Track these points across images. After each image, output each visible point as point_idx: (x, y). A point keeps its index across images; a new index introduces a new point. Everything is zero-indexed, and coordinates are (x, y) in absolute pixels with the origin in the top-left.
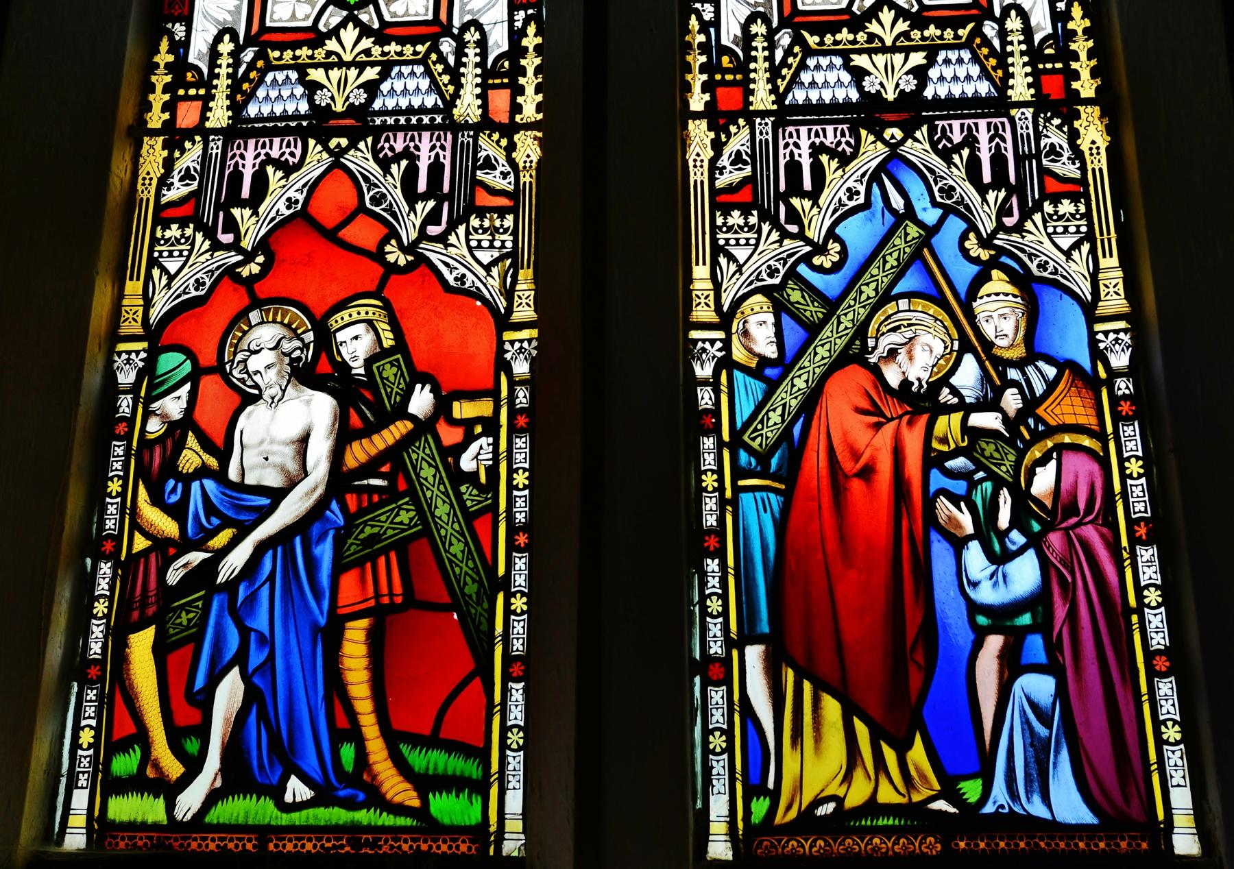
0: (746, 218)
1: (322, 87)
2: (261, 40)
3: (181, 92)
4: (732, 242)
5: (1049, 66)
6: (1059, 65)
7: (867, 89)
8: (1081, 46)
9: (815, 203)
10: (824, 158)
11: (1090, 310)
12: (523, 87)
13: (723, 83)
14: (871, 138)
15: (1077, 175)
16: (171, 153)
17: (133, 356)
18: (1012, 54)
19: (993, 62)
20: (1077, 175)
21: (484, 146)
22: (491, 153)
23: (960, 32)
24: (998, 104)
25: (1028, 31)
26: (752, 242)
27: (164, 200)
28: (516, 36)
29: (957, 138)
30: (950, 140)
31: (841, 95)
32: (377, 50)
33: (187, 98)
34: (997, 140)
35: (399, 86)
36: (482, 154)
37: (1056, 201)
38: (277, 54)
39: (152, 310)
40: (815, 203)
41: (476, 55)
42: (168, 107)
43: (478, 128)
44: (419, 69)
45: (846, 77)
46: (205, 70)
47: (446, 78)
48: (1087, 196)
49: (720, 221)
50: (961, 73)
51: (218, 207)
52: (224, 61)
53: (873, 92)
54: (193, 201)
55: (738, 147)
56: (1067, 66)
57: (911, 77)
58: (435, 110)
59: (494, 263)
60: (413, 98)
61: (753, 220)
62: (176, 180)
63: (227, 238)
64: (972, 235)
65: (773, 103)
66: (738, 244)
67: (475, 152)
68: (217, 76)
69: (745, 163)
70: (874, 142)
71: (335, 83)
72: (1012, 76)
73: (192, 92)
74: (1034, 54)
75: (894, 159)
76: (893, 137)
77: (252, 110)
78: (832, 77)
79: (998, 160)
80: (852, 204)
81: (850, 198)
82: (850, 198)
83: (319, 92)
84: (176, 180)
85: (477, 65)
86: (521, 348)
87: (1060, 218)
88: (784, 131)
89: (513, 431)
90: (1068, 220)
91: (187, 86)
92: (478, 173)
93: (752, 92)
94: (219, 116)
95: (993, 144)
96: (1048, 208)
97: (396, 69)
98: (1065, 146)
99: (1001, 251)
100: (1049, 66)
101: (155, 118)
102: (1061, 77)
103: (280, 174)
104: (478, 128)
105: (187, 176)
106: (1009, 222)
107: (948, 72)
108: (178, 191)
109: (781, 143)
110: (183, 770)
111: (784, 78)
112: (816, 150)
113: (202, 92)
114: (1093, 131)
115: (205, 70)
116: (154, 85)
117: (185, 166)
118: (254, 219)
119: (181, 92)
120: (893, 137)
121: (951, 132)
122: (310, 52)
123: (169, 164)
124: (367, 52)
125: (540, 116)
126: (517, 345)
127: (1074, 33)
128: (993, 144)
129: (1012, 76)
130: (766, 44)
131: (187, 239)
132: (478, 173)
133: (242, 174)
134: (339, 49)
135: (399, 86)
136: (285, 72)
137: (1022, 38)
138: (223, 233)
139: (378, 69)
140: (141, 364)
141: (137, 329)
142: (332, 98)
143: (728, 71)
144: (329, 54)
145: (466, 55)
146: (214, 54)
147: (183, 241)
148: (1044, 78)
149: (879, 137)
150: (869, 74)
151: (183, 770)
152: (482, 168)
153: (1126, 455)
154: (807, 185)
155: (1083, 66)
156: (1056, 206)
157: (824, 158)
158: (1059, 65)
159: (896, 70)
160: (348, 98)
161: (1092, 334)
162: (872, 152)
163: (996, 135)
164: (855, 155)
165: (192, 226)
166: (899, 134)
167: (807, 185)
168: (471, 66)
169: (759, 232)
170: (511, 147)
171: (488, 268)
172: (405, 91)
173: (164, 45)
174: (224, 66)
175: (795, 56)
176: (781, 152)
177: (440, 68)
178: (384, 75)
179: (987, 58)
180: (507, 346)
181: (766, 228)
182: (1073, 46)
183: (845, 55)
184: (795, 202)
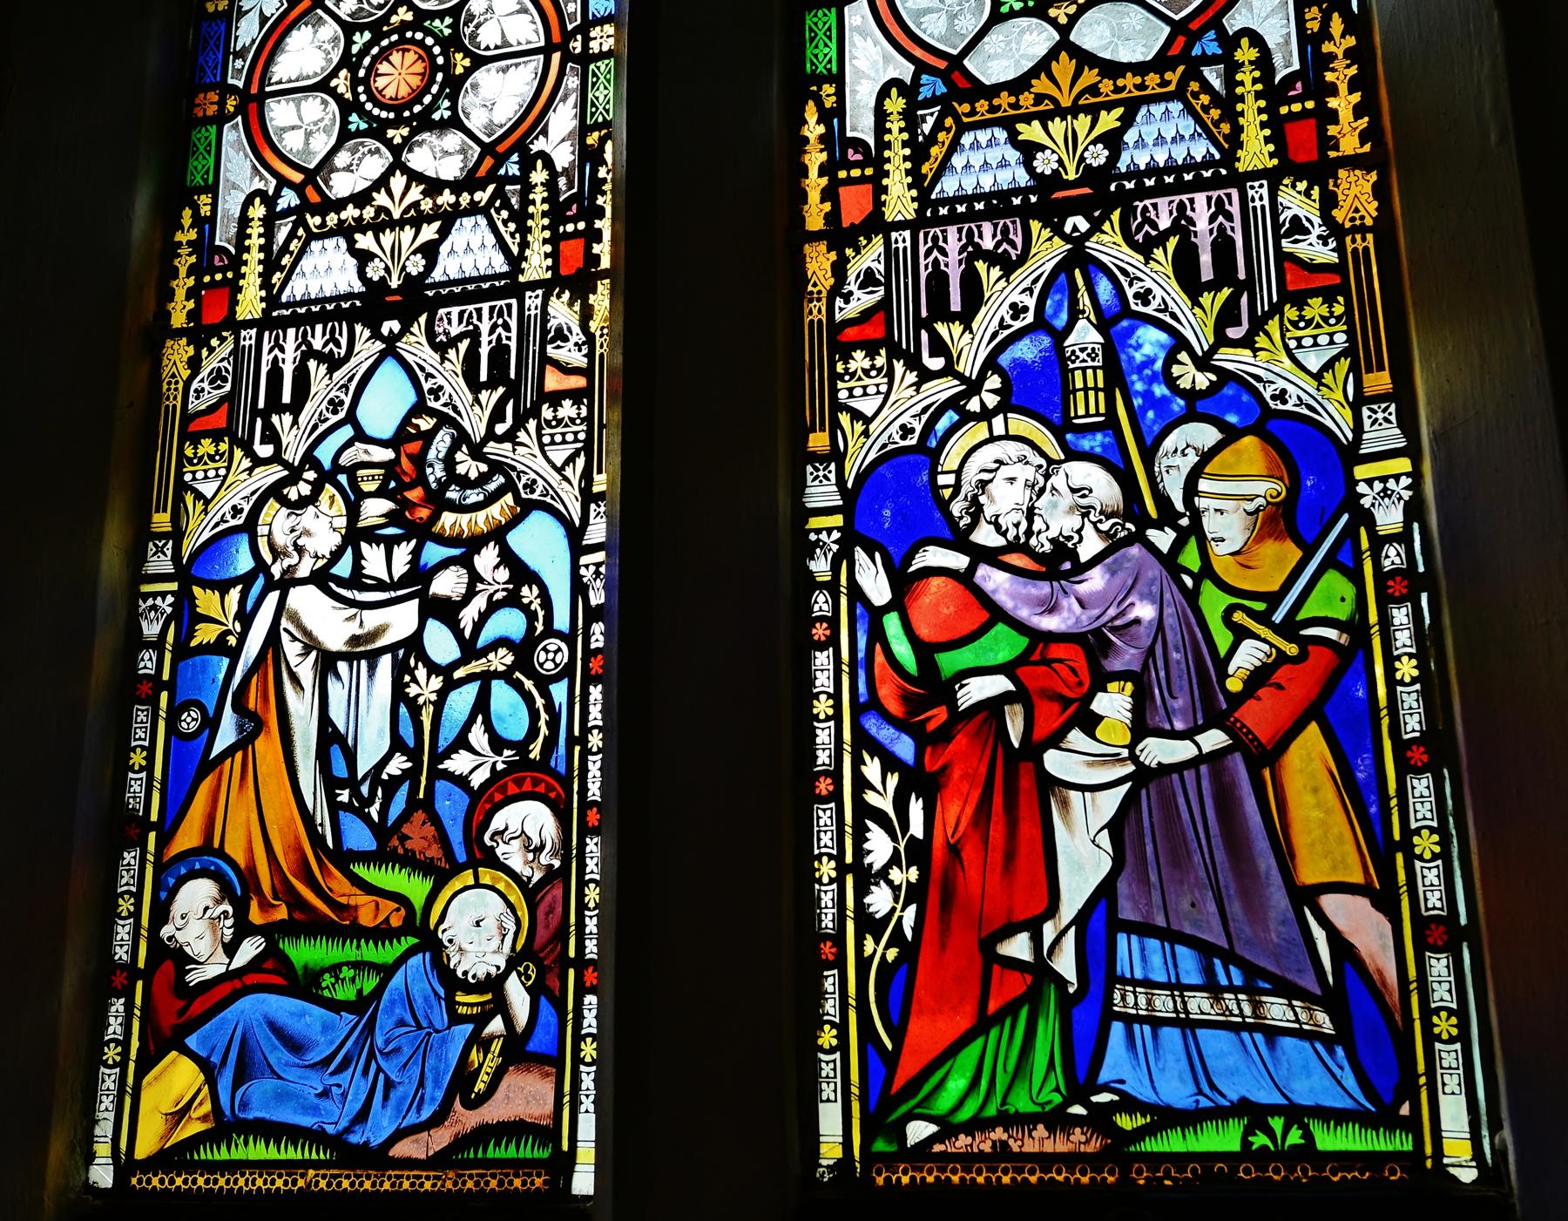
0: (1331, 307)
1: (1043, 148)
2: (946, 91)
3: (842, 174)
4: (1307, 342)
5: (1296, 107)
6: (1310, 105)
7: (1039, 170)
8: (1341, 74)
9: (968, 328)
10: (981, 266)
11: (575, 534)
12: (1335, 112)
13: (850, 181)
14: (1046, 233)
15: (1334, 258)
16: (841, 255)
17: (1391, 484)
18: (1241, 99)
19: (1215, 113)
20: (1334, 258)
21: (1286, 203)
22: (1296, 211)
23: (1168, 76)
24: (1223, 173)
25: (1264, 62)
26: (883, 388)
27: (838, 317)
28: (1309, 42)
29: (1164, 223)
30: (1154, 226)
31: (1004, 179)
32: (1106, 86)
33: (850, 181)
34: (935, 253)
35: (1150, 135)
36: (1286, 215)
37: (1300, 301)
38: (966, 108)
39: (185, 542)
40: (968, 328)
41: (1255, 81)
42: (829, 194)
43: (1273, 178)
44: (1175, 107)
45: (1013, 155)
46: (872, 143)
47: (1215, 113)
48: (1344, 289)
49: (840, 368)
50: (1169, 134)
51: (920, 324)
52: (895, 125)
53: (1048, 172)
54: (880, 316)
55: (868, 264)
56: (1321, 104)
57: (1100, 146)
58: (1208, 163)
59: (1329, 365)
60: (1192, 145)
61: (880, 361)
62: (852, 286)
63: (936, 364)
64: (1183, 356)
65: (1272, 155)
66: (865, 394)
67: (1275, 215)
68: (888, 146)
69: (878, 283)
70: (1050, 239)
71: (1061, 142)
72: (887, 174)
73: (856, 173)
74: (1273, 94)
75: (1078, 258)
76: (1075, 228)
77: (948, 186)
78: (994, 156)
79: (1222, 246)
80: (1018, 325)
81: (1015, 317)
82: (1015, 317)
83: (1039, 155)
84: (853, 287)
85: (905, 144)
86: (1385, 489)
87: (1309, 323)
88: (926, 235)
89: (588, 680)
90: (1318, 326)
91: (850, 165)
92: (1284, 243)
93: (885, 190)
94: (900, 202)
95: (1215, 225)
96: (1291, 313)
97: (1143, 110)
98: (1317, 221)
99: (1225, 376)
100: (1296, 107)
101: (814, 210)
102: (1312, 122)
103: (996, 272)
104: (1273, 178)
105: (868, 280)
106: (1234, 333)
107: (976, 159)
108: (862, 300)
109: (922, 250)
110: (591, 1192)
111: (505, 223)
112: (974, 253)
113: (869, 171)
114: (1357, 193)
115: (872, 143)
116: (806, 167)
117: (865, 267)
118: (967, 336)
119: (842, 174)
120: (1075, 228)
121: (981, 236)
122: (1012, 100)
123: (839, 270)
124: (1093, 90)
125: (1367, 148)
126: (1378, 486)
127: (1332, 57)
128: (1215, 225)
129: (887, 174)
130: (1257, 74)
131: (880, 370)
132: (1284, 241)
133: (946, 276)
134: (1054, 92)
135: (1150, 135)
136: (989, 131)
137: (902, 124)
138: (931, 356)
139: (1119, 111)
140: (835, 547)
141: (169, 568)
142: (1060, 161)
143: (856, 164)
144: (1039, 99)
145: (890, 131)
146: (881, 115)
147: (1332, 321)
148: (1288, 127)
149: (1058, 231)
150: (1043, 148)
151: (591, 1192)
152: (1288, 234)
153: (144, 775)
154: (956, 305)
155: (1343, 103)
156: (1301, 309)
157: (981, 266)
158: (1310, 105)
159: (1081, 139)
160: (1082, 159)
161: (575, 567)
162: (1048, 252)
163: (1220, 209)
164: (1023, 258)
165: (883, 352)
166: (1083, 225)
167: (956, 305)
168: (1250, 99)
169: (890, 375)
170: (1328, 203)
171: (1318, 377)
172: (1160, 140)
173: (811, 114)
174: (1248, 82)
175: (948, 130)
176: (922, 263)
177: (1205, 99)
178: (1127, 121)
179: (1206, 109)
180: (1362, 488)
181: (899, 367)
182: (1329, 77)
183: (1008, 124)
184: (941, 328)
